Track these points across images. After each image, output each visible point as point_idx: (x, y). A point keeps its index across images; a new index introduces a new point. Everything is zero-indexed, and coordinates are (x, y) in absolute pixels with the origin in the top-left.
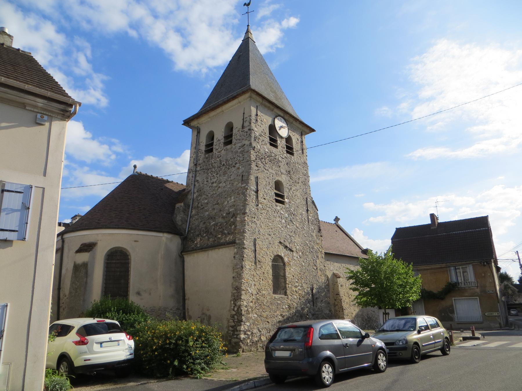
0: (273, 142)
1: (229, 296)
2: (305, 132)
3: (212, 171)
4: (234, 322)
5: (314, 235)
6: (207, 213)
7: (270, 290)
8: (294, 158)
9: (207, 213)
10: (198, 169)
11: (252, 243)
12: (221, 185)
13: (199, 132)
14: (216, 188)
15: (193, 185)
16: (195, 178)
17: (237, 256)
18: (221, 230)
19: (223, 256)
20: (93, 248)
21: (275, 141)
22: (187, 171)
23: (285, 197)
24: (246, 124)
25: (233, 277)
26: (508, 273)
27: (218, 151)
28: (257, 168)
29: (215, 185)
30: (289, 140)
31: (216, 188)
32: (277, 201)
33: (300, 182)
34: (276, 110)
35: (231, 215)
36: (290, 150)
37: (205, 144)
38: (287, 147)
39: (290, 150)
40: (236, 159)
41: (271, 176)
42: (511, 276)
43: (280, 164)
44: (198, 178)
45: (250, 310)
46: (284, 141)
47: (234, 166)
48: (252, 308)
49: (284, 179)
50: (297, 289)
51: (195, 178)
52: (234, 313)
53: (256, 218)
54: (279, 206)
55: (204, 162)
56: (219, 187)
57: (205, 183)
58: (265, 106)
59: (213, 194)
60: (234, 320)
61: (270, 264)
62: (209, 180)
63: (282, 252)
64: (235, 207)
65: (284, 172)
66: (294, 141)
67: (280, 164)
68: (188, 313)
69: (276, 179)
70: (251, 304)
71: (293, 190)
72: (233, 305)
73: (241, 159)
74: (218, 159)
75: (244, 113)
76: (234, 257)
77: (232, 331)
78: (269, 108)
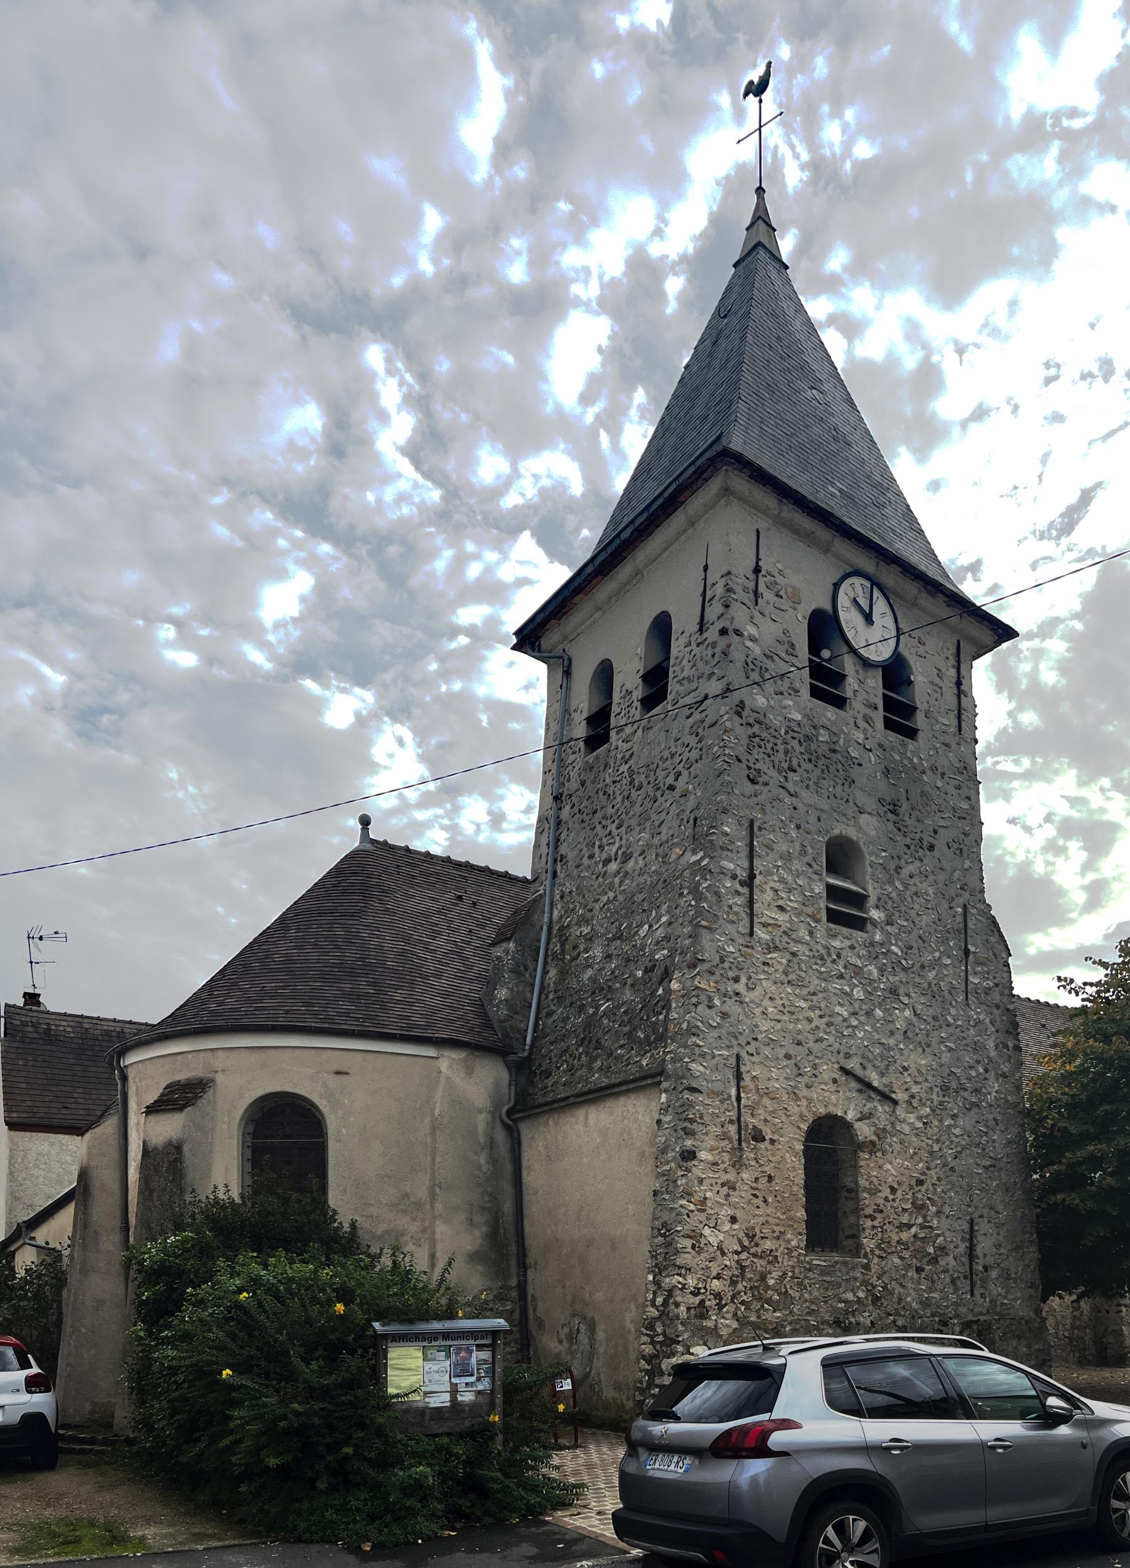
0: (827, 685)
1: (640, 1256)
2: (973, 641)
3: (605, 818)
4: (653, 1343)
5: (991, 1044)
6: (589, 973)
7: (796, 1240)
8: (919, 750)
9: (589, 973)
10: (566, 812)
11: (730, 1074)
12: (631, 864)
13: (567, 673)
14: (617, 880)
15: (549, 875)
16: (556, 848)
17: (668, 1118)
18: (627, 1029)
19: (634, 1117)
20: (197, 1097)
21: (838, 678)
22: (535, 822)
23: (872, 901)
24: (714, 611)
25: (655, 1193)
26: (721, 173)
27: (623, 735)
28: (749, 788)
29: (613, 867)
30: (895, 673)
31: (617, 880)
32: (834, 917)
33: (940, 844)
34: (842, 546)
35: (658, 972)
36: (900, 716)
37: (585, 715)
38: (889, 704)
39: (900, 716)
40: (677, 759)
41: (812, 819)
42: (551, 353)
43: (855, 772)
44: (564, 849)
45: (711, 1303)
46: (875, 681)
47: (672, 788)
48: (718, 1296)
49: (867, 830)
50: (905, 1236)
51: (556, 848)
52: (653, 1312)
53: (743, 980)
54: (841, 940)
55: (583, 784)
56: (627, 873)
57: (586, 861)
58: (796, 531)
59: (609, 901)
60: (652, 1337)
61: (800, 1147)
62: (597, 850)
63: (847, 1105)
64: (671, 944)
65: (870, 804)
66: (920, 678)
67: (855, 772)
68: (535, 1311)
69: (836, 832)
70: (716, 1284)
71: (905, 872)
72: (653, 1288)
73: (695, 754)
74: (624, 768)
75: (706, 568)
76: (659, 1122)
77: (647, 1372)
78: (809, 539)
